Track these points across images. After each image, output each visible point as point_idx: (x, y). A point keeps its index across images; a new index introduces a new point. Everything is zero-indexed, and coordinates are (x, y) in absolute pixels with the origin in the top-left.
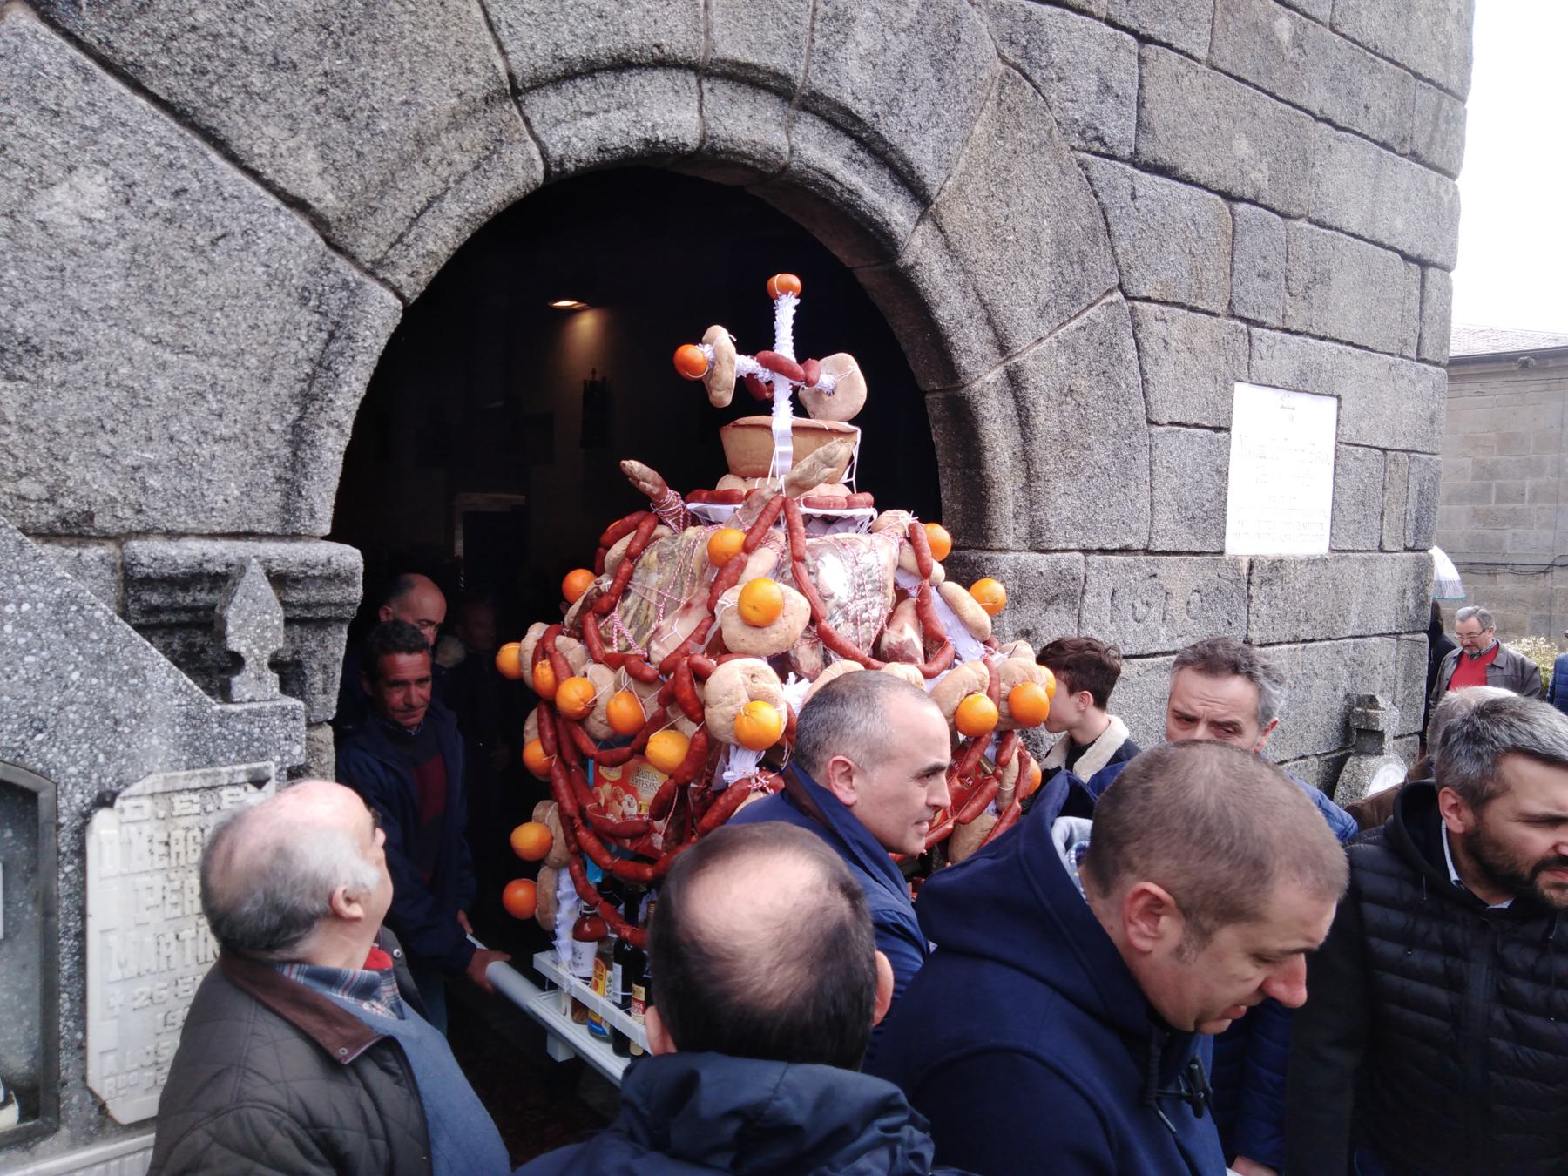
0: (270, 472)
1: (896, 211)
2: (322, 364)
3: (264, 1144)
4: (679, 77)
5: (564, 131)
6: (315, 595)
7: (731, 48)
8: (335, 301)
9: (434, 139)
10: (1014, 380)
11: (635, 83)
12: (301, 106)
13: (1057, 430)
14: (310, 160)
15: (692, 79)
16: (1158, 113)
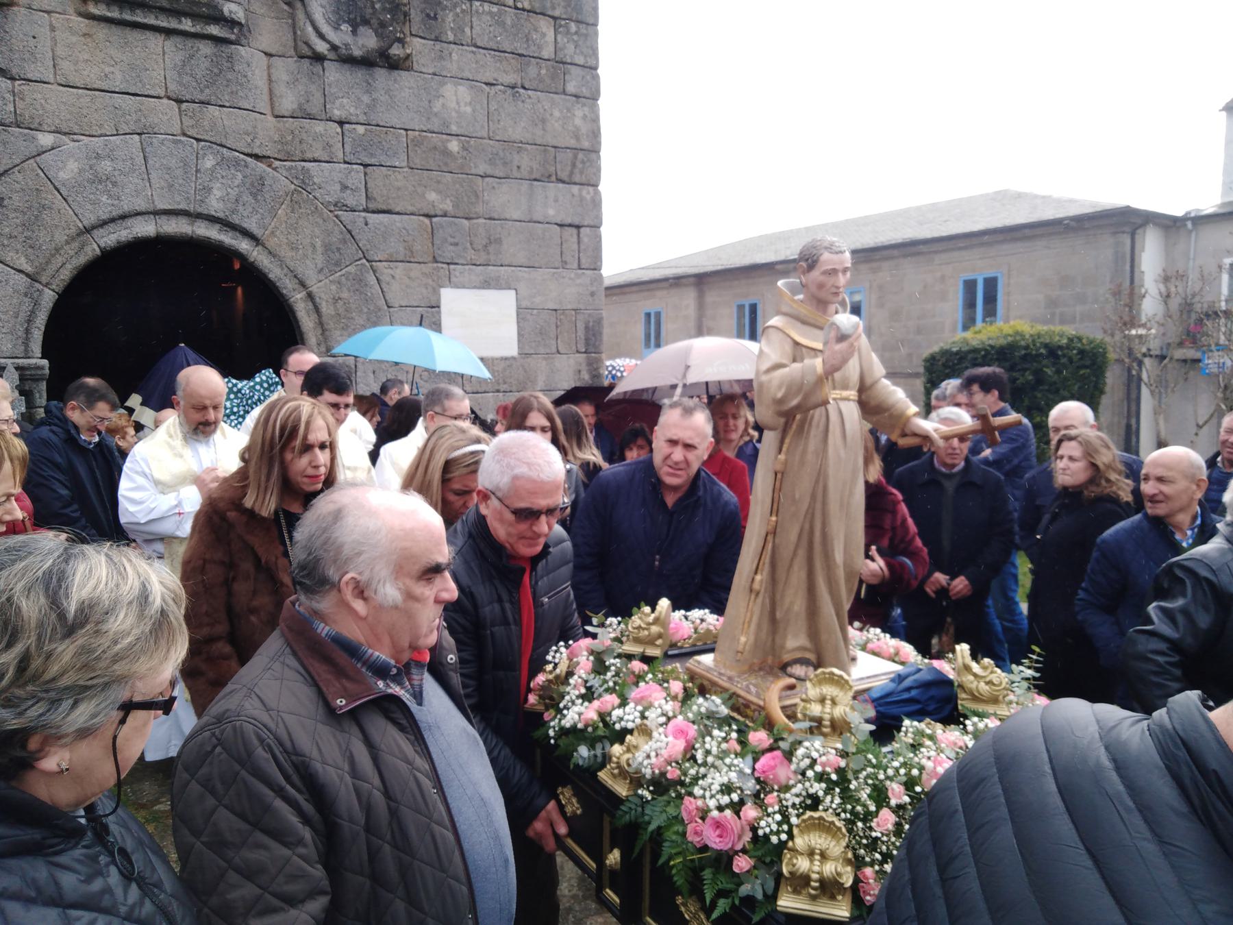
0: (20, 341)
1: (244, 246)
2: (33, 312)
3: (250, 754)
4: (146, 217)
5: (105, 239)
6: (33, 372)
7: (161, 206)
8: (35, 295)
9: (62, 248)
10: (310, 296)
11: (129, 222)
12: (19, 246)
13: (333, 313)
14: (23, 260)
15: (152, 217)
16: (375, 193)
